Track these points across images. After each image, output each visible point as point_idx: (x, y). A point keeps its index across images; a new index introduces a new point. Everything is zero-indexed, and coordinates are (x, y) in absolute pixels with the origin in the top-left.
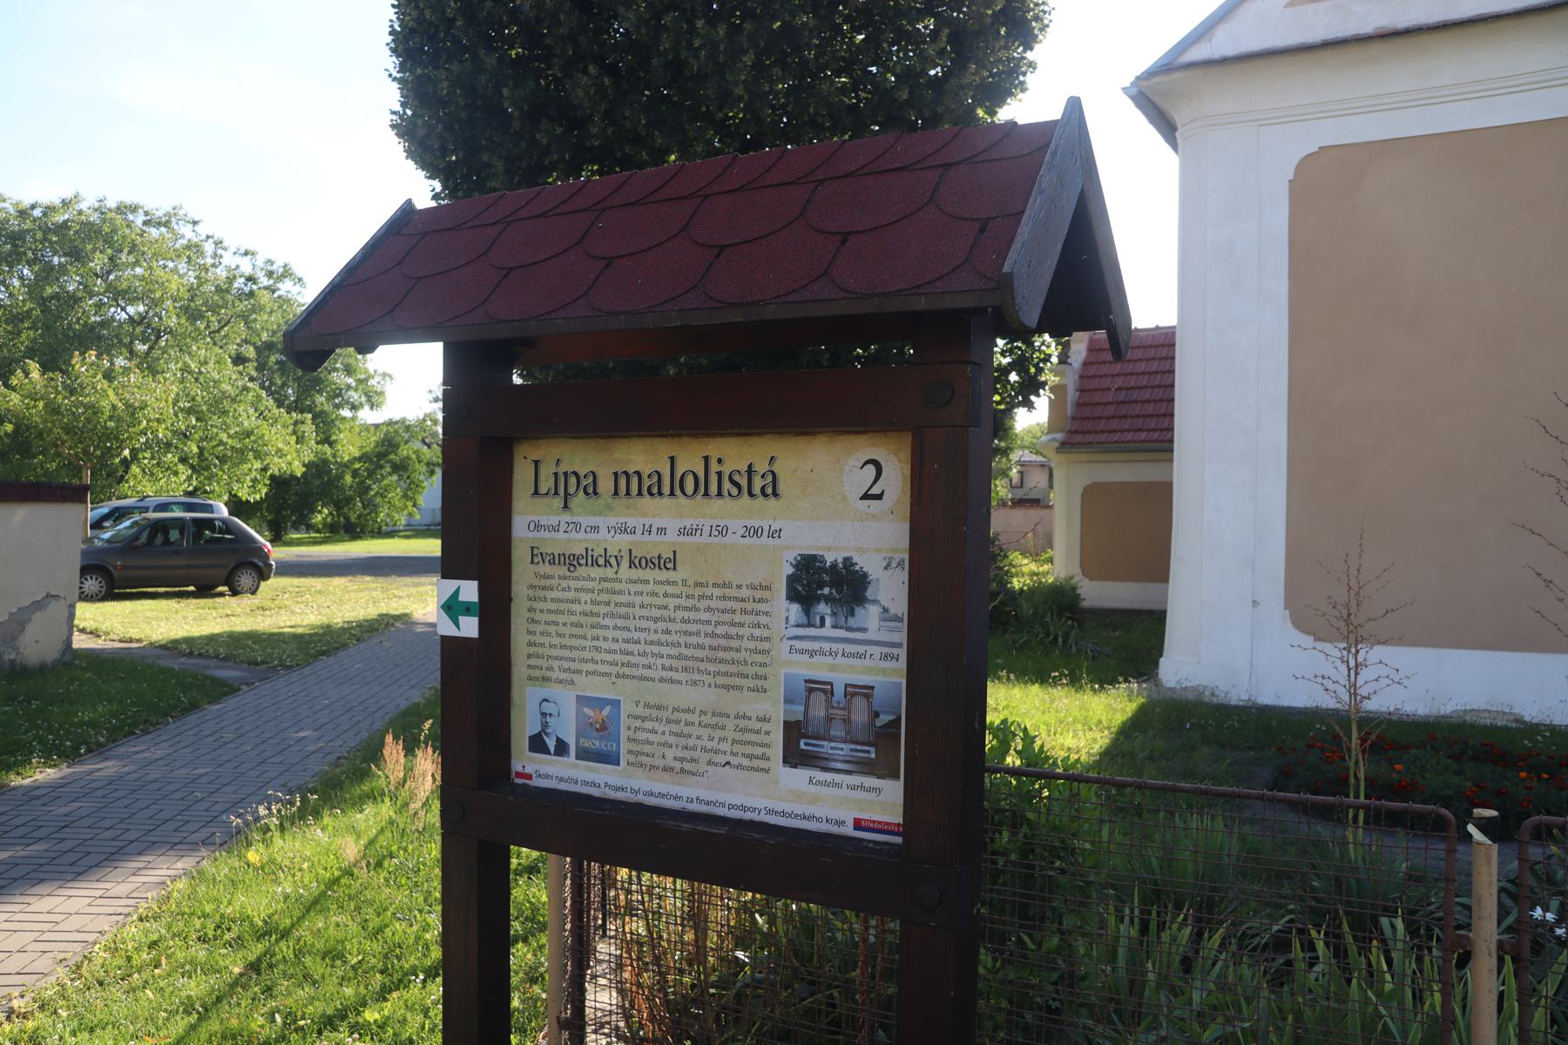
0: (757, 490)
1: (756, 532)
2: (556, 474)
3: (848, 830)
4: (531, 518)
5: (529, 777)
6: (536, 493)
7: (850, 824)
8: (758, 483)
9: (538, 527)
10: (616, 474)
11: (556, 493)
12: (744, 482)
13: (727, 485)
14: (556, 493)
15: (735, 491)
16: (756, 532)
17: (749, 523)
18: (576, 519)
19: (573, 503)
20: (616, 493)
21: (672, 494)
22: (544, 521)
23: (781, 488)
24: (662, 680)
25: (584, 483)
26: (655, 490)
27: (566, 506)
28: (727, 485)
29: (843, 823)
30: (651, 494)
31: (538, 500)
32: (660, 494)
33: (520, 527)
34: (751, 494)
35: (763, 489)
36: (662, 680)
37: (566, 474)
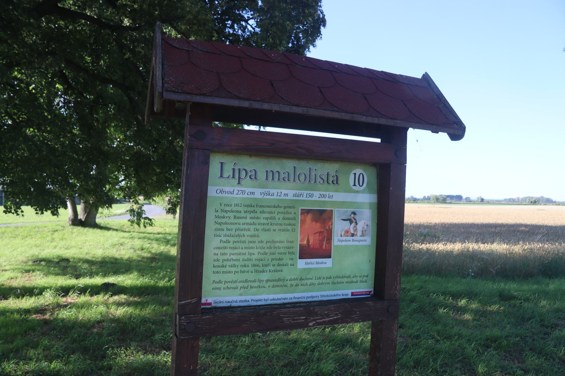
0: (330, 182)
1: (324, 196)
2: (234, 169)
3: (350, 296)
4: (218, 188)
5: (210, 304)
6: (221, 176)
7: (350, 294)
8: (331, 179)
9: (222, 192)
10: (267, 171)
11: (233, 177)
12: (326, 179)
13: (319, 179)
14: (233, 177)
15: (322, 182)
16: (324, 196)
17: (321, 193)
18: (243, 189)
19: (242, 182)
20: (267, 179)
21: (294, 181)
22: (227, 189)
23: (339, 182)
24: (236, 282)
25: (249, 174)
26: (335, 182)
27: (239, 183)
28: (319, 179)
29: (348, 294)
30: (333, 183)
31: (222, 179)
32: (289, 180)
33: (212, 191)
34: (328, 183)
35: (333, 181)
36: (236, 282)
37: (239, 169)
